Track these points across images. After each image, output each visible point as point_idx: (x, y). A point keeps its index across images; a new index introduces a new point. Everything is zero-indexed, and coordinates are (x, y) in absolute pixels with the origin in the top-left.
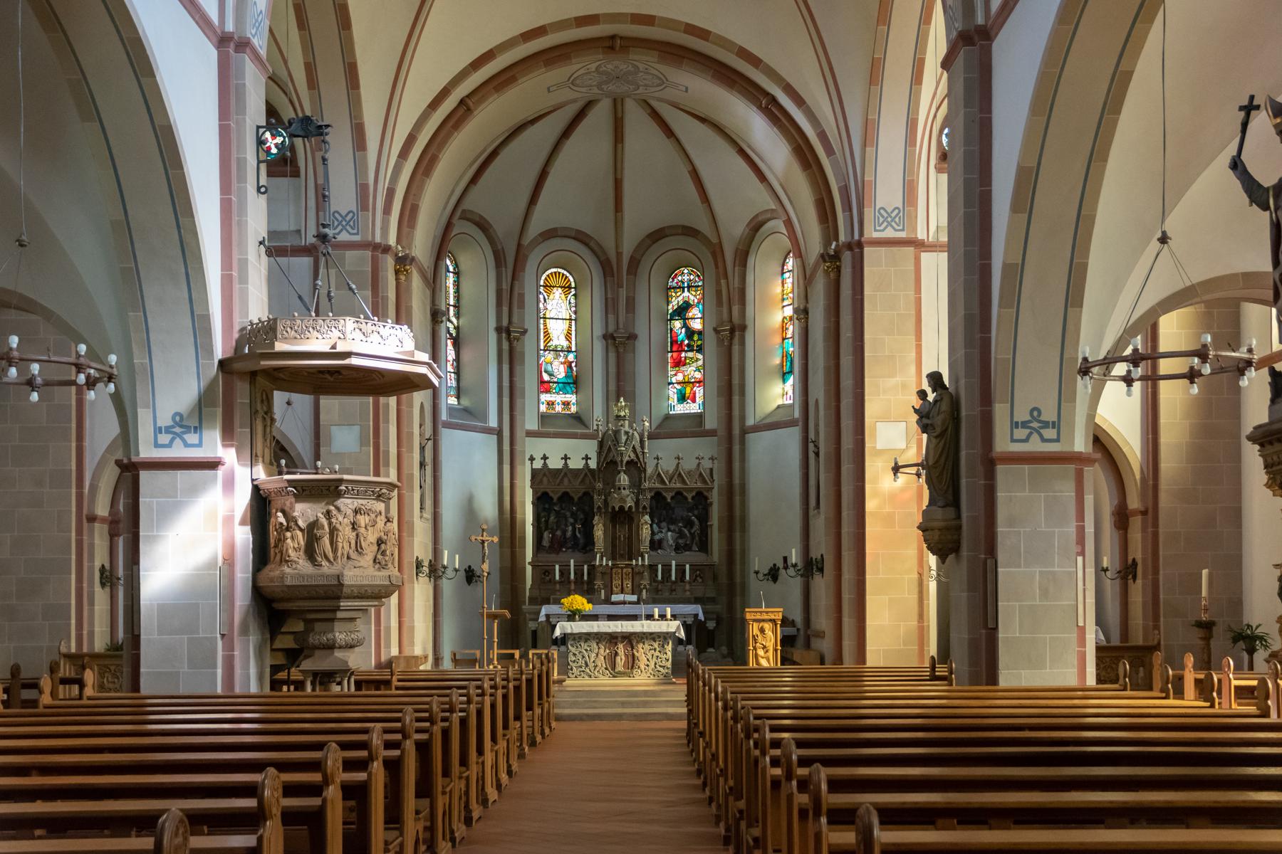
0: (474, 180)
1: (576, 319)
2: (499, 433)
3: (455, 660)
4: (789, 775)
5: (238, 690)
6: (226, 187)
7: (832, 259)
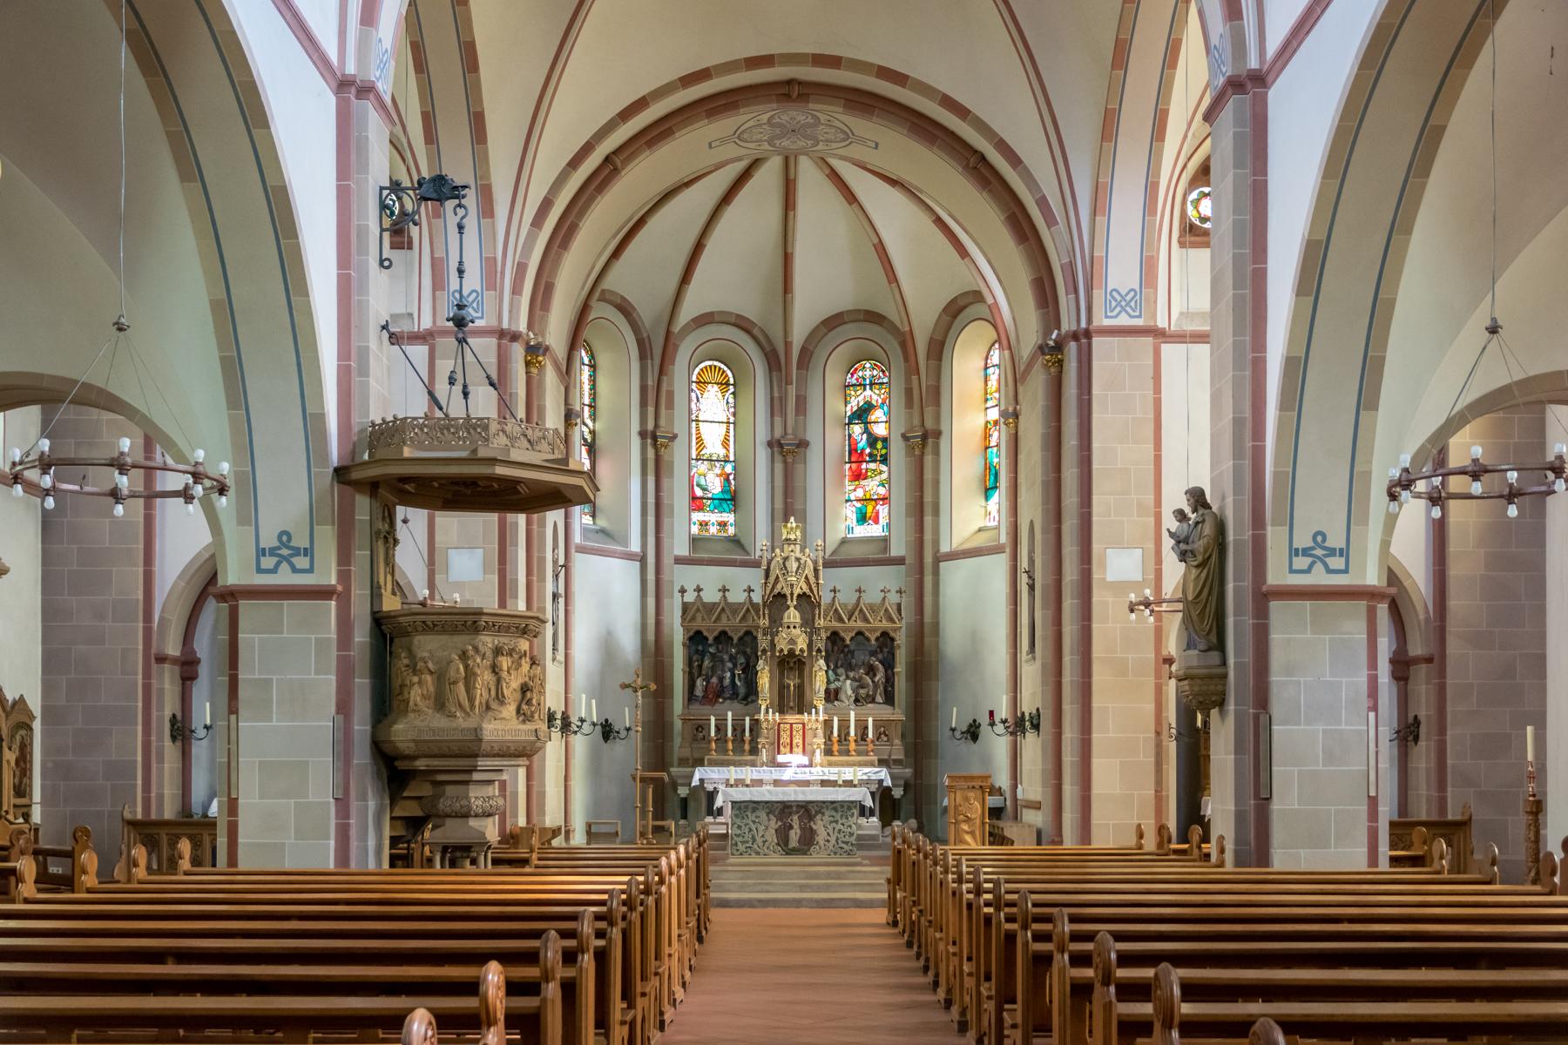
0: (616, 254)
1: (735, 421)
2: (643, 560)
3: (590, 835)
4: (1107, 979)
5: (353, 867)
6: (344, 260)
7: (1053, 352)
